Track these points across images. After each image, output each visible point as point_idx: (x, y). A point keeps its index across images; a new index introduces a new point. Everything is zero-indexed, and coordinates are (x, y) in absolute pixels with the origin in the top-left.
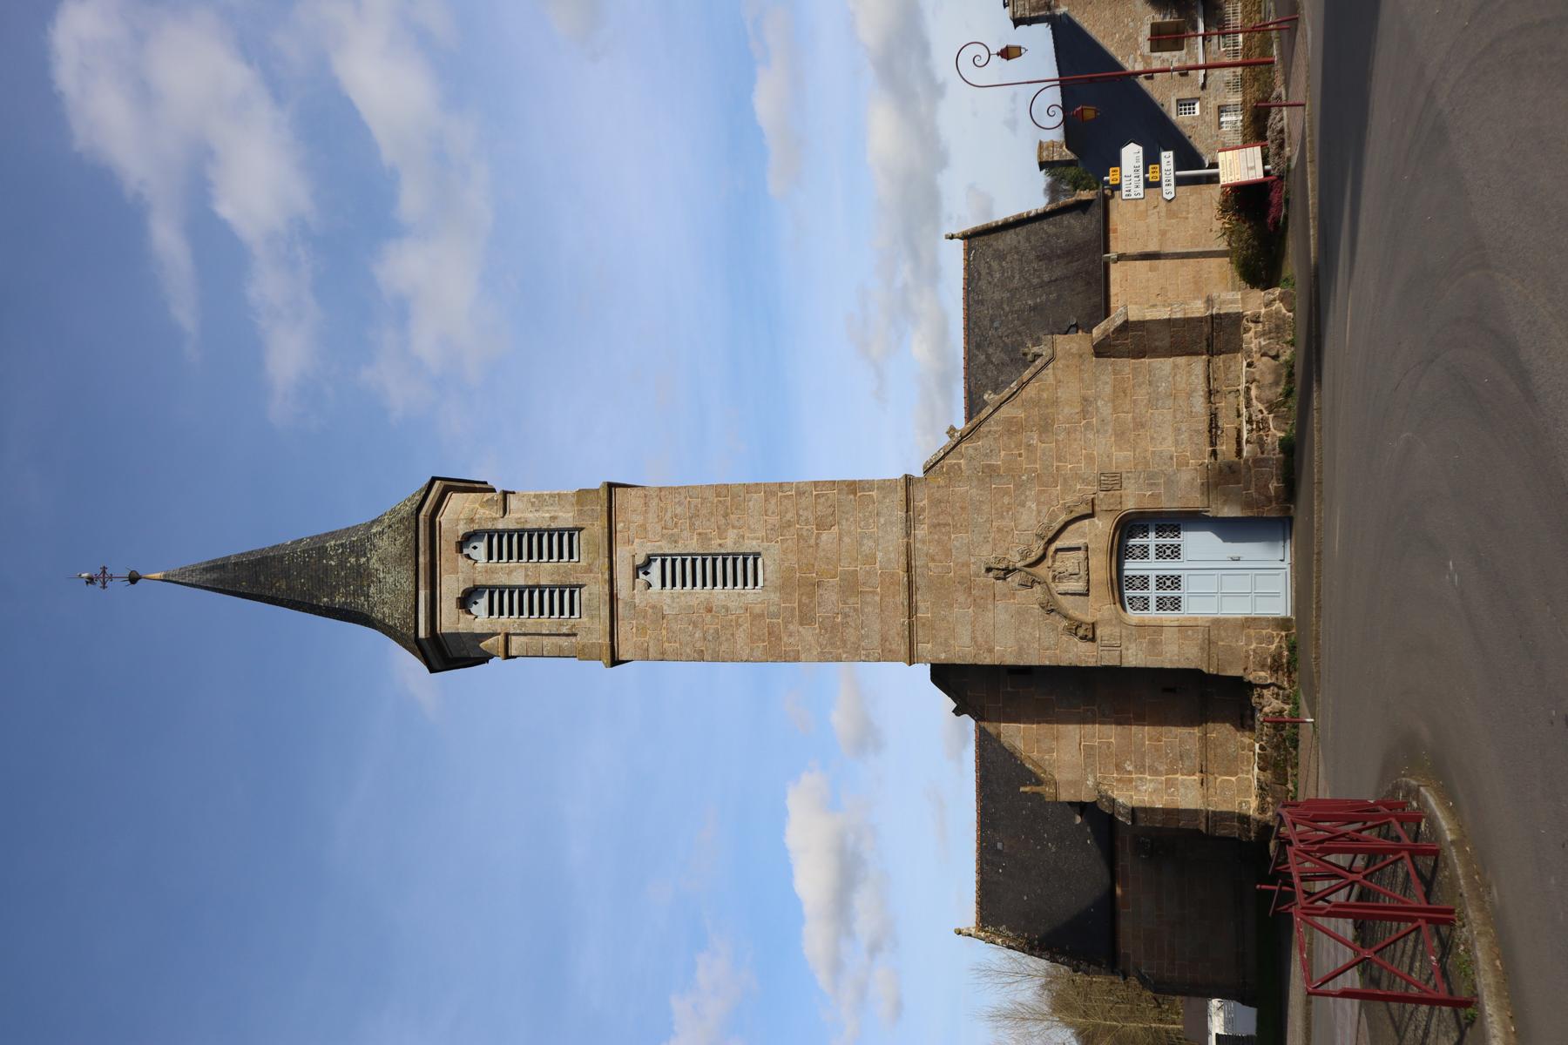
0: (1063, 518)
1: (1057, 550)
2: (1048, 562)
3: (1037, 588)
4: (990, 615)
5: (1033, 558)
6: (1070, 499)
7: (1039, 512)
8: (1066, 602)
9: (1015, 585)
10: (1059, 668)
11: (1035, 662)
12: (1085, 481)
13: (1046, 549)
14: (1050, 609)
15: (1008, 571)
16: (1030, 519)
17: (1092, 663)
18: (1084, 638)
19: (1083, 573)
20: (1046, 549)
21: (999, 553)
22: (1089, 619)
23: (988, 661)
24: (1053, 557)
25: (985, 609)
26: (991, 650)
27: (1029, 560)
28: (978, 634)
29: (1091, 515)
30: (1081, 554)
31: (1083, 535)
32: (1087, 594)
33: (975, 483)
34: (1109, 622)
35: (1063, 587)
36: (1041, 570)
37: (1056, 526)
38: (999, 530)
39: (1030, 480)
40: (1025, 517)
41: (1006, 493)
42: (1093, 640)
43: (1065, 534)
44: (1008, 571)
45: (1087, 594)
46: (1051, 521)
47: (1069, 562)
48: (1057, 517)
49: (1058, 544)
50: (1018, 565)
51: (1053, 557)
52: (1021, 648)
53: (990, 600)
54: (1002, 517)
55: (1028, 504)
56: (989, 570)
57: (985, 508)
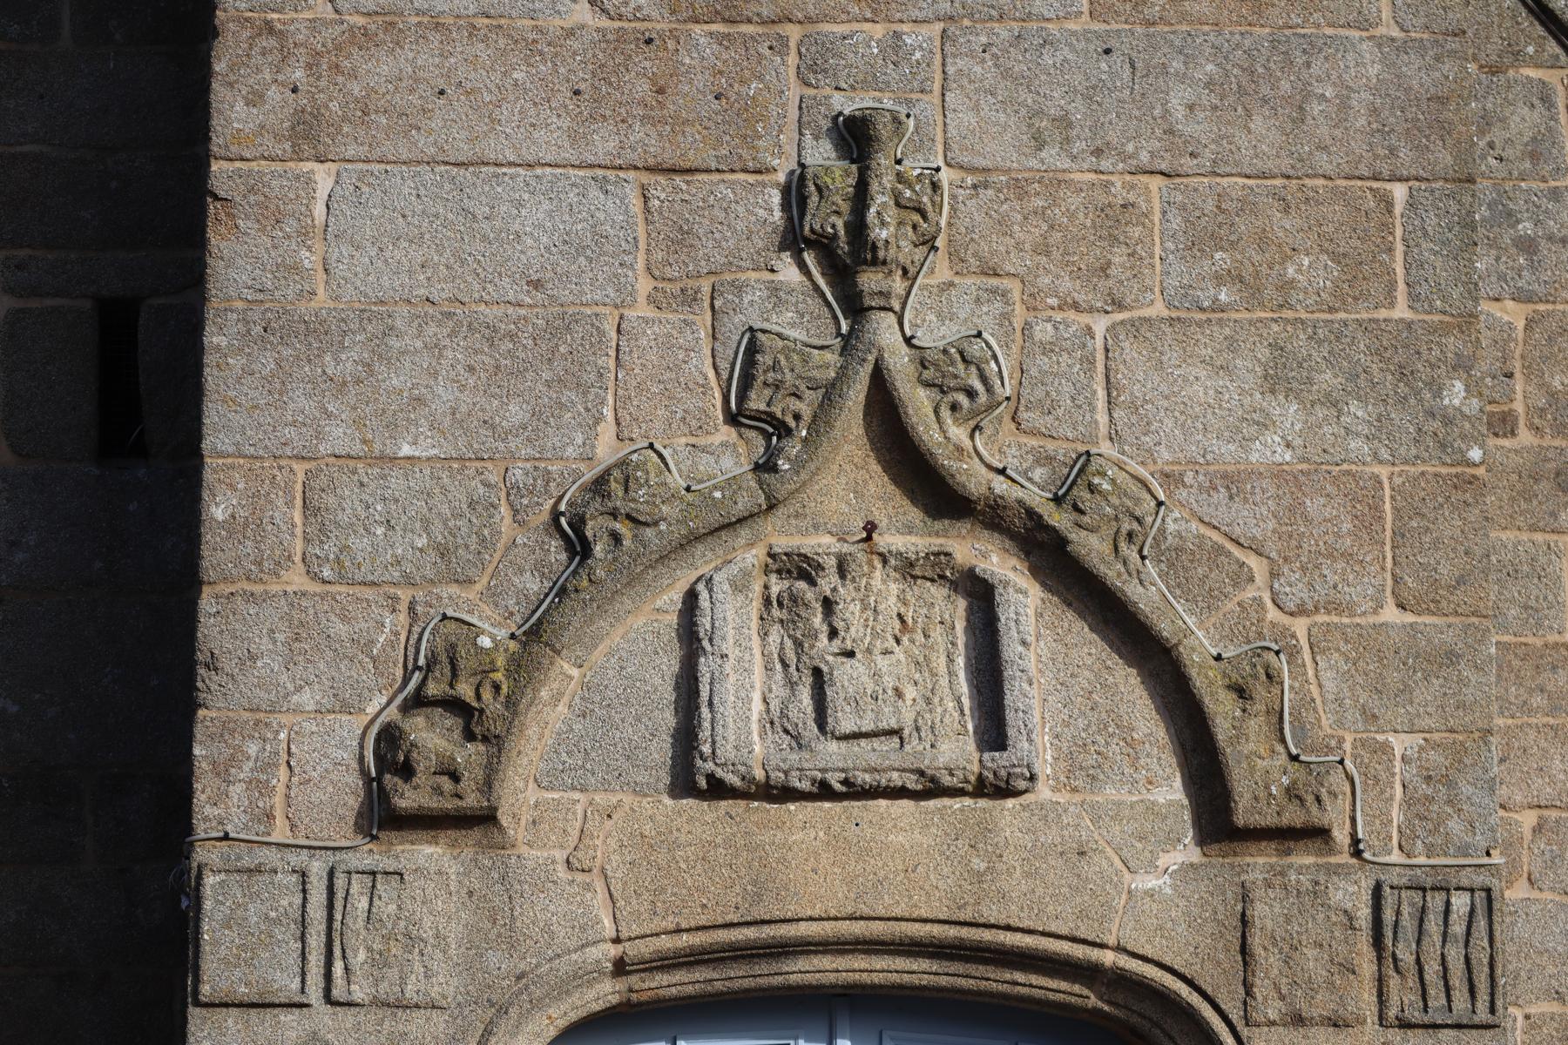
0: (1200, 640)
1: (981, 595)
2: (908, 532)
3: (728, 457)
4: (550, 141)
5: (938, 431)
6: (1320, 686)
7: (1233, 483)
8: (627, 642)
9: (751, 309)
10: (178, 578)
11: (226, 428)
12: (1436, 788)
13: (990, 516)
14: (589, 535)
15: (845, 264)
16: (1189, 423)
17: (218, 806)
18: (390, 754)
19: (832, 757)
20: (990, 516)
21: (961, 210)
22: (521, 794)
23: (233, 115)
24: (938, 569)
25: (590, 102)
26: (307, 134)
27: (918, 403)
28: (423, 57)
29: (1216, 820)
30: (957, 751)
31: (1082, 770)
32: (691, 778)
33: (1418, 74)
34: (496, 923)
35: (735, 622)
36: (845, 486)
37: (1147, 592)
38: (1115, 219)
39: (1443, 433)
40: (1200, 386)
41: (1359, 273)
42: (381, 817)
43: (1088, 647)
44: (845, 264)
45: (691, 778)
46: (1175, 559)
47: (901, 670)
48: (1208, 601)
49: (1025, 601)
50: (884, 331)
51: (938, 569)
52: (318, 334)
53: (646, 141)
54: (1197, 243)
55: (1289, 414)
56: (855, 137)
57: (1261, 138)
